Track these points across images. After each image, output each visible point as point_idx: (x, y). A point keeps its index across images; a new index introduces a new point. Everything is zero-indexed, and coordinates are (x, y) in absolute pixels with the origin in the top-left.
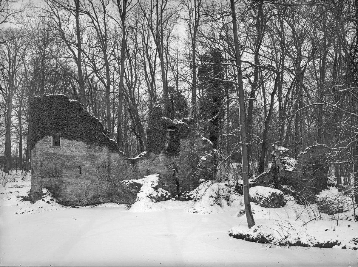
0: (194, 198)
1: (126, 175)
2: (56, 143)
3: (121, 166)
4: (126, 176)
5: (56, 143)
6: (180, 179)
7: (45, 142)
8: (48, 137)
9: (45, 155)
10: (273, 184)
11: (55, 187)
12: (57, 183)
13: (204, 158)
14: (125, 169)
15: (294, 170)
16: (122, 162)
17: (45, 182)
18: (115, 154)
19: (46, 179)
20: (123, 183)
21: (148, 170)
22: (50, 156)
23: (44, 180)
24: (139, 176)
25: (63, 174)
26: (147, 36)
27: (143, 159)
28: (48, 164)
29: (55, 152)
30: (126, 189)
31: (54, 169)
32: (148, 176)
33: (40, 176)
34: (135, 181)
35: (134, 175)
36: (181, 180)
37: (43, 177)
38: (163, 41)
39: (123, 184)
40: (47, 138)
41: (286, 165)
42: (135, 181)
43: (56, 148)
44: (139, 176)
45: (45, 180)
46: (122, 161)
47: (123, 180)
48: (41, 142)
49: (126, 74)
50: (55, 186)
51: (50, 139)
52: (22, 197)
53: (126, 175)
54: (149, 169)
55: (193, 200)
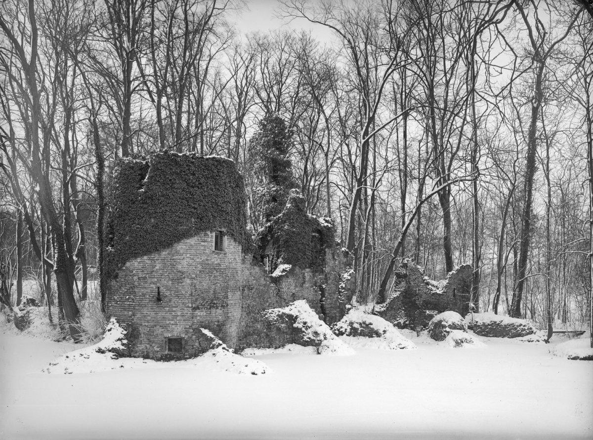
0: (346, 332)
1: (267, 302)
2: (219, 246)
3: (261, 288)
4: (268, 304)
5: (219, 246)
6: (327, 306)
7: (203, 243)
8: (209, 233)
9: (200, 267)
10: (403, 310)
11: (217, 325)
12: (220, 317)
13: (346, 276)
14: (266, 292)
15: (444, 292)
16: (262, 281)
17: (198, 318)
18: (255, 267)
19: (202, 311)
20: (266, 314)
21: (293, 294)
22: (208, 269)
23: (198, 312)
24: (283, 304)
25: (229, 302)
26: (287, 73)
27: (288, 277)
28: (200, 282)
29: (219, 261)
30: (274, 324)
31: (212, 292)
32: (295, 302)
33: (190, 305)
34: (282, 310)
35: (277, 301)
36: (328, 308)
37: (195, 309)
38: (35, 7)
39: (266, 316)
40: (206, 235)
41: (430, 286)
42: (282, 310)
43: (221, 255)
44: (283, 304)
45: (199, 314)
46: (263, 279)
47: (264, 310)
48: (192, 241)
49: (38, 74)
50: (216, 323)
51: (212, 236)
52: (110, 351)
53: (267, 302)
54: (294, 291)
55: (345, 335)
